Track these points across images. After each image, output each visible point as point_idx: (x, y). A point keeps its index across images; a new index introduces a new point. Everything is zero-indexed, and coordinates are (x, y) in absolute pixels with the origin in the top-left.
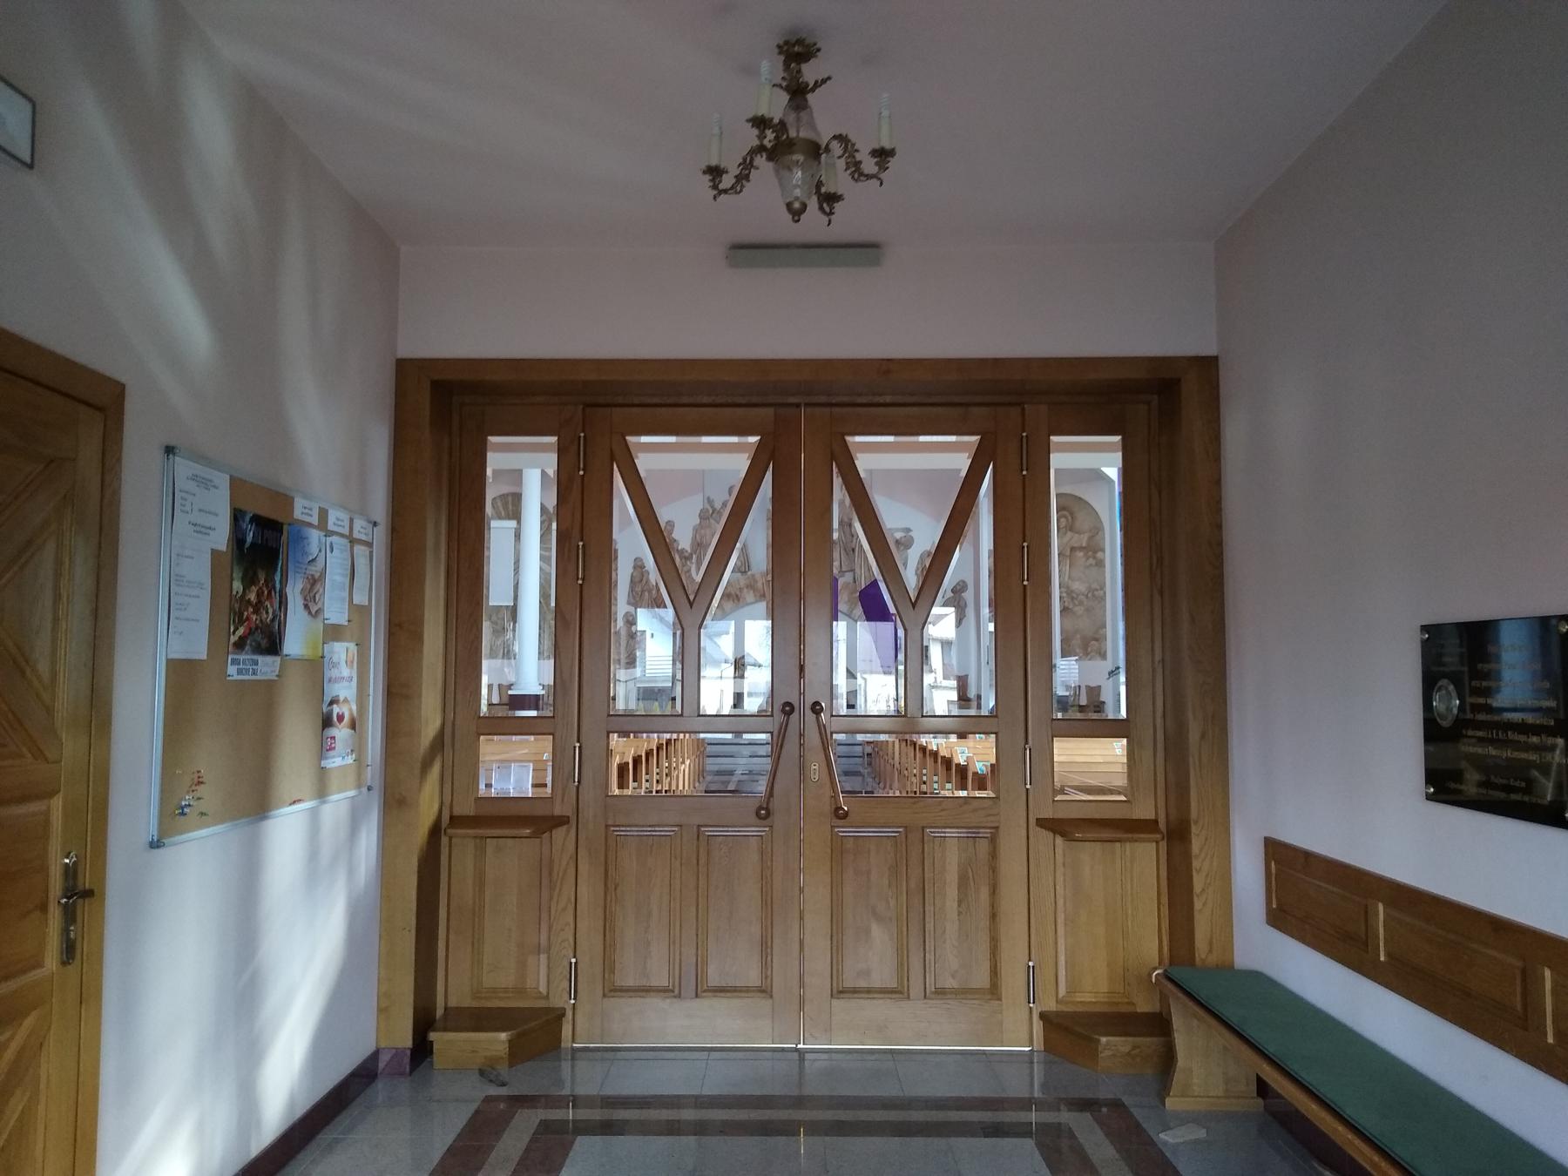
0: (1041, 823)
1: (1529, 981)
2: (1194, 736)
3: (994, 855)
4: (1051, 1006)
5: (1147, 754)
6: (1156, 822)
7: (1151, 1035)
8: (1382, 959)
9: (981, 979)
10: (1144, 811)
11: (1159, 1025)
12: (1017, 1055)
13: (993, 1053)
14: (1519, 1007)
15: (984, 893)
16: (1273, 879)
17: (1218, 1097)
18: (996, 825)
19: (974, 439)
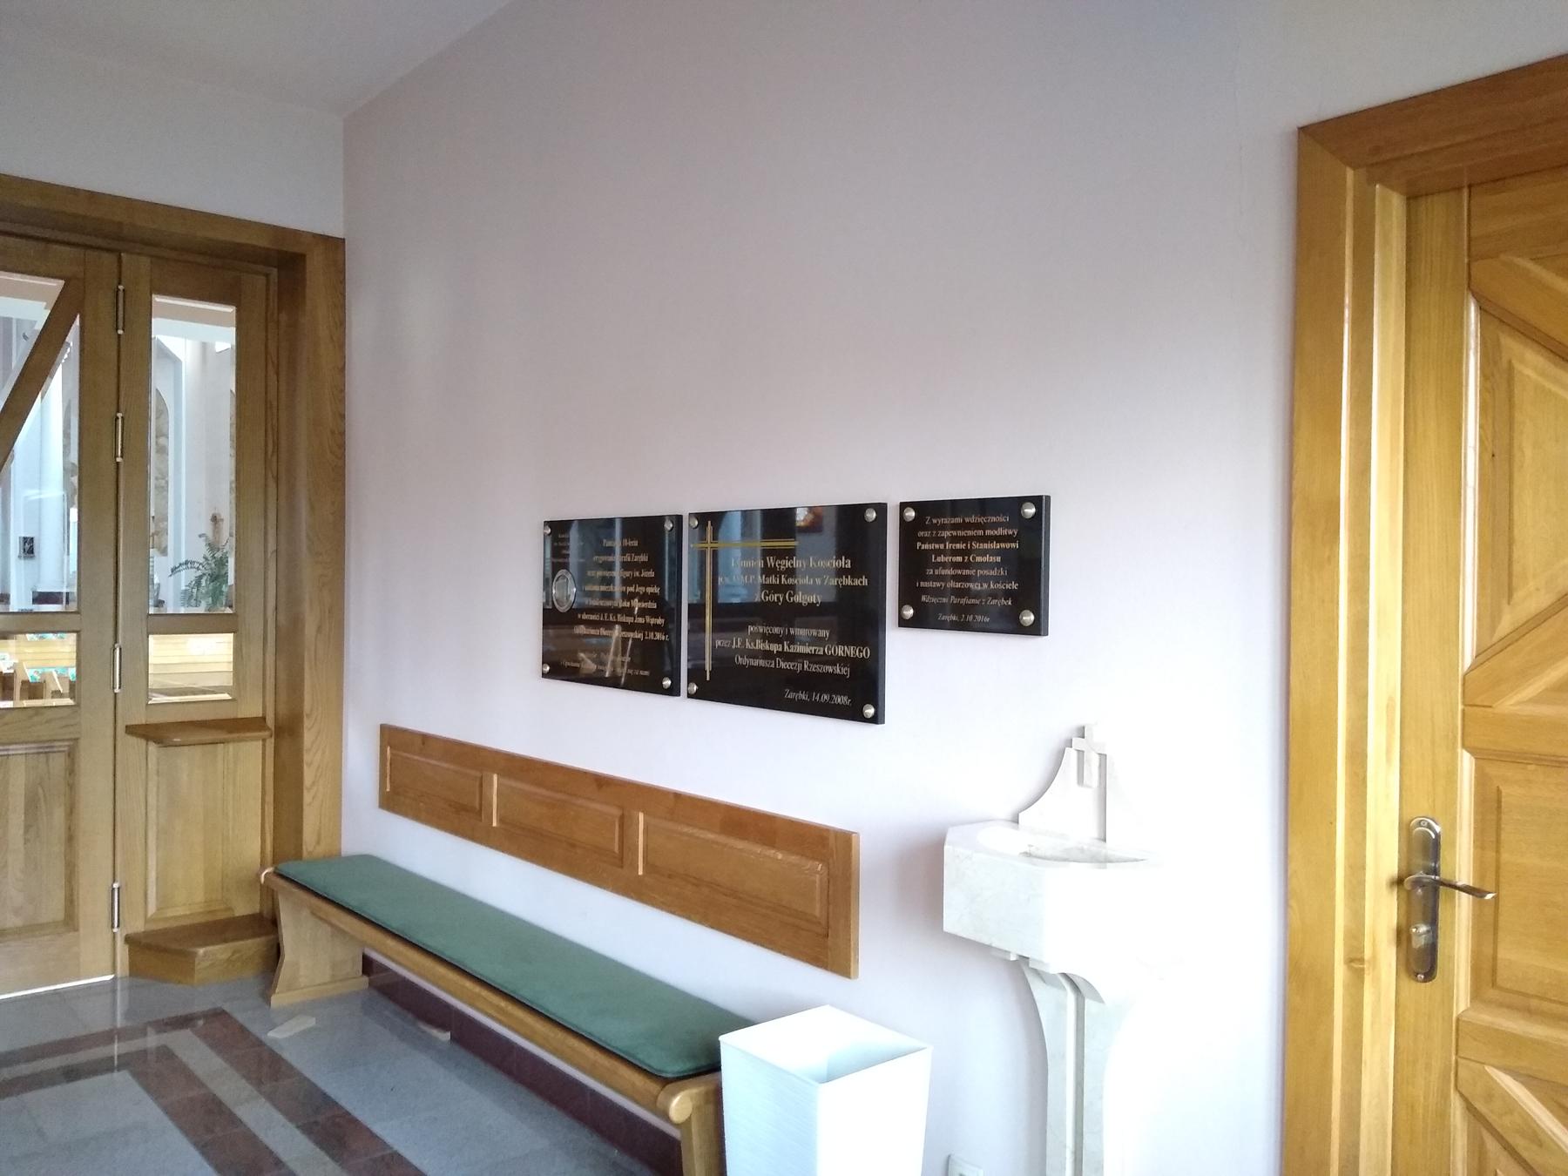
0: (131, 730)
1: (625, 823)
2: (310, 629)
3: (71, 770)
4: (137, 926)
5: (255, 651)
6: (264, 718)
7: (254, 936)
8: (495, 824)
9: (53, 909)
10: (251, 708)
11: (267, 924)
12: (52, 994)
13: (66, 991)
14: (616, 849)
15: (59, 814)
16: (388, 764)
17: (325, 984)
18: (77, 736)
19: (56, 285)
